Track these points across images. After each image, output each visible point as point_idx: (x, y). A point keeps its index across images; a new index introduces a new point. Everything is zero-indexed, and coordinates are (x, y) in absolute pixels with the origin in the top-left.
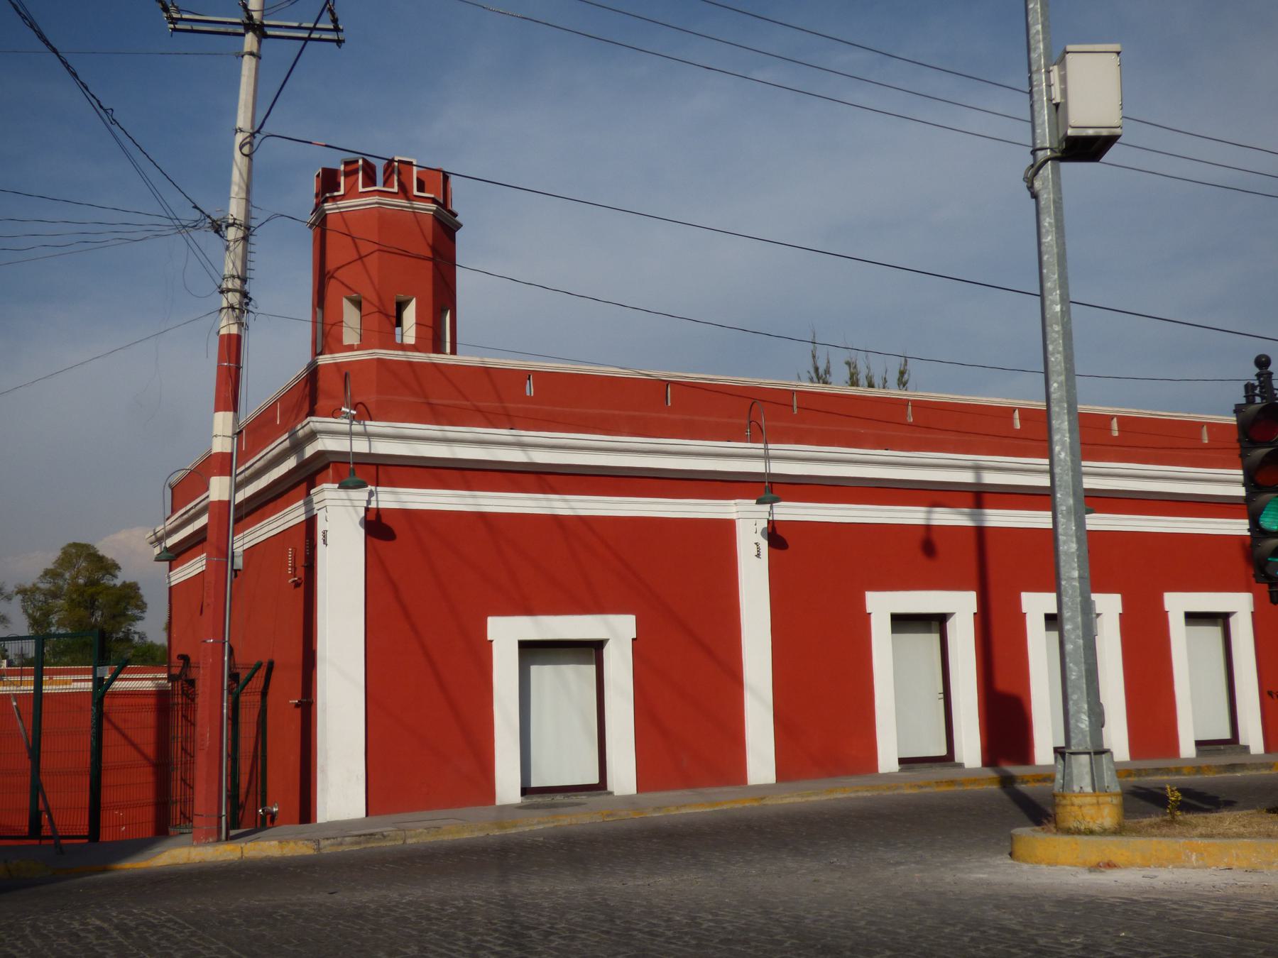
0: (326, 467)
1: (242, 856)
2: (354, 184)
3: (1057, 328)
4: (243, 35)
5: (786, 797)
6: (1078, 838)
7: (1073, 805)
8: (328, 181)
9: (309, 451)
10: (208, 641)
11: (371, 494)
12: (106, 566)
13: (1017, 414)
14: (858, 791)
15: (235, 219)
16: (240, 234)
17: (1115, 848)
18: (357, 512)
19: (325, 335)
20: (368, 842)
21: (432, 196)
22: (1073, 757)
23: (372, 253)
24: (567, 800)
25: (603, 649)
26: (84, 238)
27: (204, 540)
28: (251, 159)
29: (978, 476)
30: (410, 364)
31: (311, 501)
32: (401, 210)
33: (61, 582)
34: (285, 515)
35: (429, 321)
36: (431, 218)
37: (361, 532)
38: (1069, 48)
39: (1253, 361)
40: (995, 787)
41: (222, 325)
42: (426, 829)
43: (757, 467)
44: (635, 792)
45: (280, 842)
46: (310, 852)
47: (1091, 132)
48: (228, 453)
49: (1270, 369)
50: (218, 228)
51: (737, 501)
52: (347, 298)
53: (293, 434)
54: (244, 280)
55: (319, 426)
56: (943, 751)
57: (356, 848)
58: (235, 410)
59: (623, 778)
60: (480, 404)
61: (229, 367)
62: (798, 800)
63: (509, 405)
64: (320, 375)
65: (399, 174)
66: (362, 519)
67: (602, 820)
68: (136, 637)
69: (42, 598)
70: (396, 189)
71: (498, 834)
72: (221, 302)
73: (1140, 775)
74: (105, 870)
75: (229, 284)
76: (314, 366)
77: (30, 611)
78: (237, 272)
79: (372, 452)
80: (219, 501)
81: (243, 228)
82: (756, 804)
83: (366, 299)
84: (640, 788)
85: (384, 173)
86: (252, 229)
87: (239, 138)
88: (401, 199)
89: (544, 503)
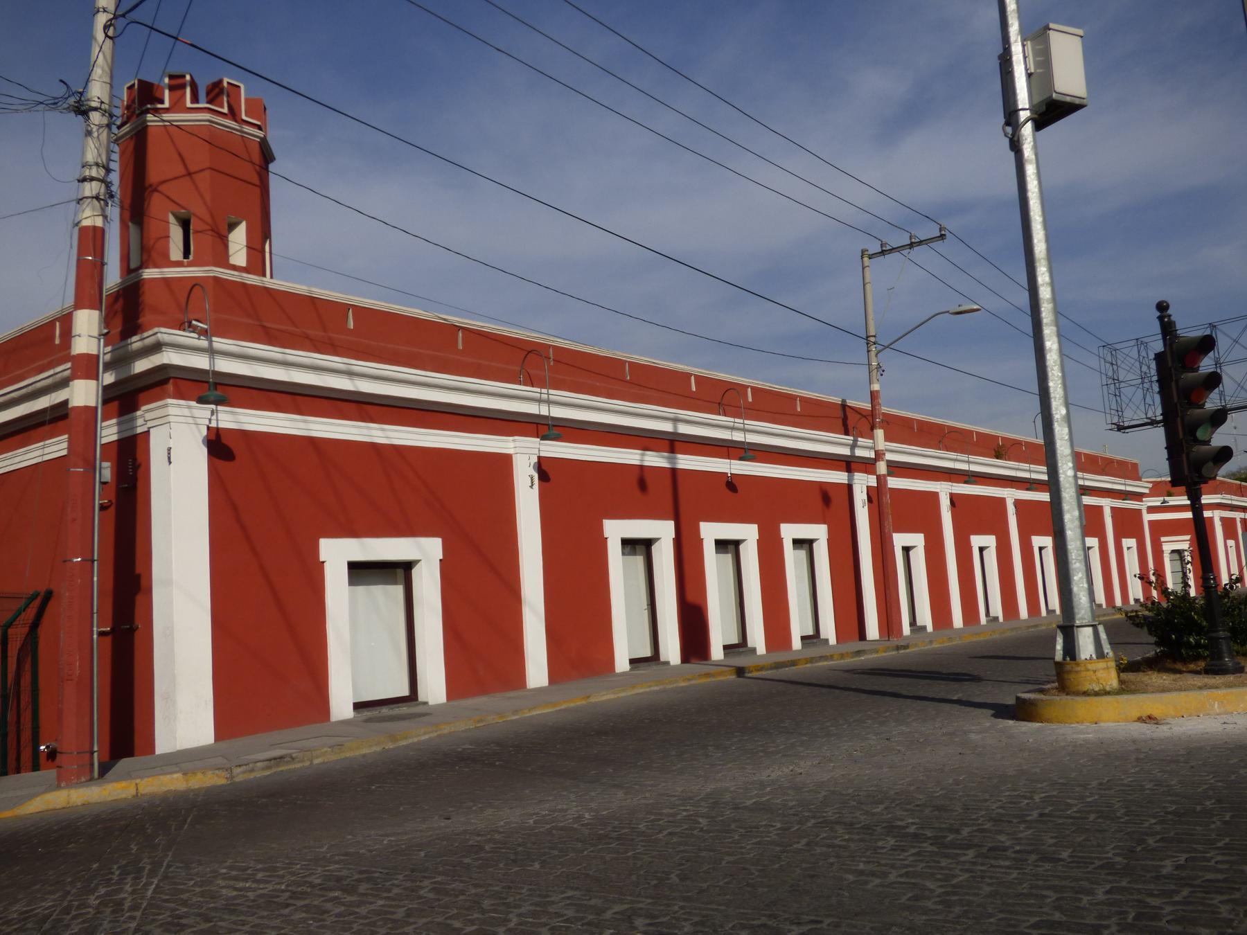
0: (165, 382)
1: (137, 793)
5: (604, 695)
7: (1088, 670)
9: (141, 366)
10: (75, 560)
14: (650, 686)
15: (102, 102)
16: (105, 121)
18: (200, 432)
20: (278, 766)
21: (259, 123)
22: (1078, 629)
25: (411, 569)
28: (114, 43)
29: (675, 427)
30: (244, 285)
31: (134, 419)
36: (257, 146)
37: (204, 451)
38: (1052, 26)
39: (1155, 306)
40: (733, 677)
41: (85, 216)
42: (330, 747)
44: (445, 701)
45: (185, 774)
47: (1068, 99)
49: (1169, 312)
50: (82, 111)
51: (516, 438)
52: (171, 213)
57: (267, 773)
59: (434, 687)
61: (93, 263)
62: (612, 696)
65: (228, 96)
66: (204, 437)
67: (474, 727)
70: (225, 110)
71: (391, 747)
73: (811, 662)
75: (94, 172)
76: (136, 280)
78: (102, 160)
79: (541, 413)
81: (107, 114)
82: (584, 702)
83: (194, 215)
84: (682, 663)
86: (115, 118)
87: (102, 19)
88: (230, 120)
89: (365, 432)
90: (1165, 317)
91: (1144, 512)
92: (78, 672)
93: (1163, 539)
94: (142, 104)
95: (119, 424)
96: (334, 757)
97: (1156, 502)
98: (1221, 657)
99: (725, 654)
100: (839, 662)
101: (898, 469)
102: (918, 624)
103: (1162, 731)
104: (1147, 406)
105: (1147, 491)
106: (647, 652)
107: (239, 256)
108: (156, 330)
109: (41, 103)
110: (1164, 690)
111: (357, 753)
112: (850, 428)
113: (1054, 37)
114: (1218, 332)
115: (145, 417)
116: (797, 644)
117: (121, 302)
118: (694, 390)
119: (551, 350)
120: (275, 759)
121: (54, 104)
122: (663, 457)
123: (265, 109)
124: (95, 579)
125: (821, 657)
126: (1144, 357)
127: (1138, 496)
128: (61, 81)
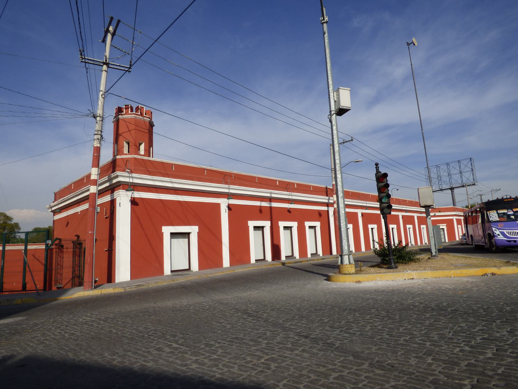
0: (120, 185)
1: (101, 293)
2: (127, 112)
3: (337, 153)
4: (103, 66)
6: (351, 275)
8: (119, 110)
9: (114, 181)
11: (132, 193)
13: (277, 182)
14: (254, 268)
15: (100, 115)
16: (101, 119)
17: (359, 277)
18: (129, 198)
19: (118, 151)
20: (139, 287)
21: (149, 117)
23: (132, 130)
24: (182, 273)
26: (53, 115)
28: (104, 99)
29: (271, 195)
30: (143, 160)
31: (114, 195)
32: (140, 120)
34: (103, 199)
35: (147, 149)
40: (281, 265)
41: (95, 144)
42: (154, 282)
43: (226, 191)
46: (123, 291)
47: (345, 108)
48: (96, 179)
49: (379, 166)
50: (95, 117)
52: (125, 141)
54: (101, 132)
55: (119, 174)
56: (263, 258)
59: (195, 267)
60: (160, 171)
61: (97, 156)
62: (242, 270)
64: (117, 161)
65: (140, 110)
70: (139, 114)
73: (307, 262)
74: (56, 300)
80: (93, 193)
82: (233, 272)
85: (136, 109)
86: (104, 118)
87: (101, 93)
89: (176, 197)
90: (377, 167)
92: (89, 261)
94: (118, 113)
95: (111, 196)
98: (391, 264)
99: (311, 256)
100: (317, 261)
102: (375, 248)
103: (361, 285)
104: (439, 185)
106: (290, 254)
107: (142, 152)
108: (116, 172)
109: (85, 115)
110: (385, 273)
111: (162, 284)
112: (328, 194)
113: (341, 91)
115: (116, 193)
116: (309, 256)
117: (112, 164)
118: (278, 184)
119: (233, 175)
120: (138, 285)
121: (88, 116)
123: (151, 113)
124: (95, 237)
125: (311, 260)
126: (438, 171)
128: (89, 110)
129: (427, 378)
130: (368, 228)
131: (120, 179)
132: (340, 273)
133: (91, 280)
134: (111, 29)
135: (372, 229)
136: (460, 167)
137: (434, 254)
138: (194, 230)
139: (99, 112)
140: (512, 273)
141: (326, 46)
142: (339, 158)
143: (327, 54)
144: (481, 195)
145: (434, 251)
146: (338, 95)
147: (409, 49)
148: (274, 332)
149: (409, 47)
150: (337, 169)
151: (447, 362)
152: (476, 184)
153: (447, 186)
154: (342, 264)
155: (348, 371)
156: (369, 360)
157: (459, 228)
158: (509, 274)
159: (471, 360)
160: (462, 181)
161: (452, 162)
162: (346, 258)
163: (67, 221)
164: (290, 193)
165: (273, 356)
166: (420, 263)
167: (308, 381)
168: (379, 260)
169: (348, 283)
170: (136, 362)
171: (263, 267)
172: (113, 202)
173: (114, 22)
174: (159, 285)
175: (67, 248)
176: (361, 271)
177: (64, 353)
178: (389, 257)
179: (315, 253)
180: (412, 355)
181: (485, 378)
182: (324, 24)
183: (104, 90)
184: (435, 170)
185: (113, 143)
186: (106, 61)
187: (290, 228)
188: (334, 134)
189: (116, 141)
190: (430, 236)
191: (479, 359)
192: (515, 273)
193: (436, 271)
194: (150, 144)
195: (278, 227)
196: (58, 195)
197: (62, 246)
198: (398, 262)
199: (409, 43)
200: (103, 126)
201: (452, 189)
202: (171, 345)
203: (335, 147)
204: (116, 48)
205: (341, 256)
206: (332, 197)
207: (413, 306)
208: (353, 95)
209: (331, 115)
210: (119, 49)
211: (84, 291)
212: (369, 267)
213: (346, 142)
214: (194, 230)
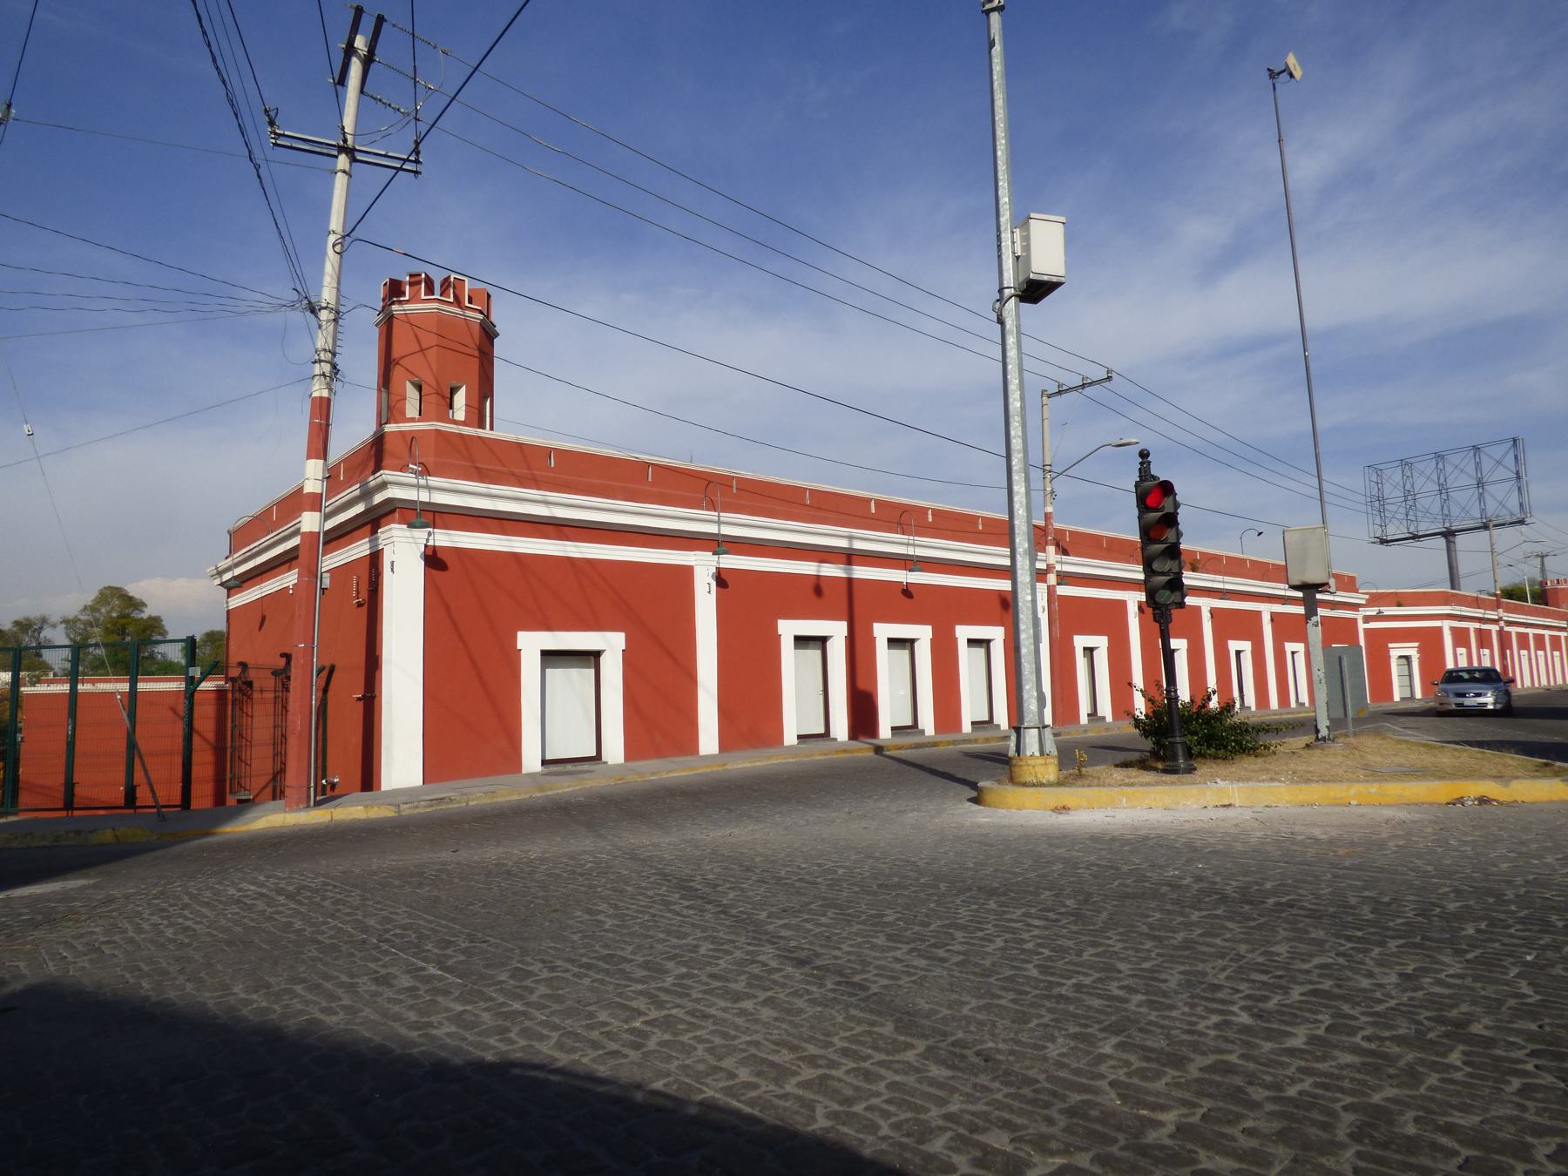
0: (393, 511)
3: (1017, 419)
4: (336, 157)
7: (1028, 765)
8: (395, 289)
9: (378, 498)
11: (429, 534)
12: (133, 603)
16: (332, 316)
17: (1066, 795)
19: (389, 408)
20: (438, 804)
24: (574, 768)
27: (296, 558)
29: (851, 544)
30: (461, 435)
31: (377, 539)
33: (97, 615)
35: (475, 403)
36: (478, 326)
38: (1032, 215)
40: (871, 754)
43: (712, 529)
45: (365, 807)
46: (391, 814)
47: (1045, 278)
50: (314, 310)
53: (364, 484)
54: (334, 354)
55: (390, 478)
56: (822, 730)
58: (325, 459)
59: (614, 751)
62: (748, 765)
63: (536, 472)
64: (387, 439)
65: (454, 288)
68: (160, 656)
69: (82, 626)
70: (451, 300)
72: (313, 370)
74: (208, 834)
77: (72, 636)
82: (720, 769)
85: (441, 286)
87: (332, 239)
91: (1360, 622)
93: (1390, 645)
95: (370, 541)
96: (489, 801)
97: (1372, 611)
98: (1174, 758)
101: (1064, 578)
103: (1063, 819)
105: (1363, 602)
108: (382, 472)
110: (1148, 784)
111: (508, 799)
114: (1482, 455)
117: (374, 449)
122: (840, 568)
123: (489, 296)
127: (1355, 607)
129: (1063, 1098)
130: (1073, 648)
131: (393, 493)
132: (1012, 780)
133: (305, 784)
134: (360, 43)
135: (1238, 653)
136: (1478, 466)
137: (1324, 732)
138: (612, 644)
139: (327, 295)
140: (1545, 799)
141: (996, 85)
142: (1020, 434)
143: (996, 108)
144: (1542, 557)
145: (1323, 724)
146: (1026, 239)
147: (1274, 89)
148: (722, 944)
149: (1274, 85)
150: (1015, 468)
151: (1153, 1056)
152: (1528, 520)
153: (1433, 526)
154: (1019, 755)
155: (852, 1065)
156: (934, 1037)
157: (1459, 656)
158: (1533, 803)
159: (1231, 1052)
160: (1483, 511)
161: (1456, 451)
162: (1031, 738)
163: (262, 613)
164: (911, 538)
165: (674, 1011)
166: (1269, 759)
167: (722, 1089)
168: (1148, 744)
169: (1029, 811)
170: (302, 1012)
171: (812, 755)
172: (375, 560)
173: (368, 23)
174: (499, 800)
175: (262, 691)
176: (1080, 776)
177: (132, 981)
178: (1170, 739)
179: (986, 719)
180: (1066, 1030)
181: (1233, 1108)
182: (991, 14)
183: (339, 230)
184: (1397, 476)
185: (376, 388)
186: (345, 141)
187: (908, 645)
188: (1008, 360)
189: (385, 381)
190: (1315, 679)
191: (1256, 1053)
192: (1555, 798)
193: (1304, 786)
194: (484, 389)
195: (872, 641)
196: (240, 537)
197: (250, 684)
198: (1202, 755)
199: (1276, 71)
200: (339, 336)
201: (1449, 534)
202: (423, 969)
203: (1011, 400)
204: (380, 100)
205: (1018, 730)
206: (1044, 551)
207: (1170, 885)
208: (1072, 241)
209: (1002, 301)
210: (390, 105)
211: (285, 812)
212: (1117, 766)
213: (1090, 384)
214: (612, 644)
